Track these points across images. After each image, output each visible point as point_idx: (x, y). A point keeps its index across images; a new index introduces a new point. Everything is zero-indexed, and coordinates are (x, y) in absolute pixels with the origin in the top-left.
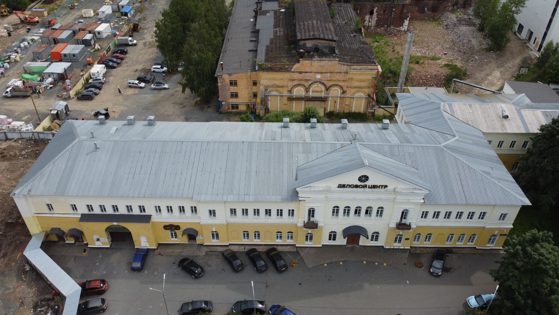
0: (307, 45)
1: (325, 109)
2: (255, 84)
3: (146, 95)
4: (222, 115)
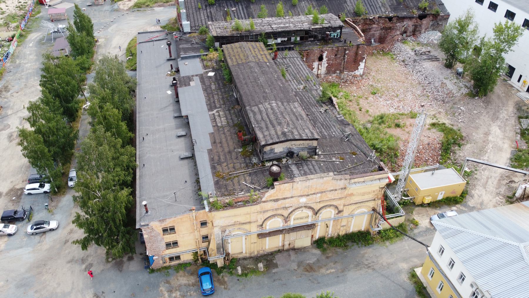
0: (276, 151)
1: (312, 236)
2: (204, 224)
3: (20, 250)
4: (155, 274)
